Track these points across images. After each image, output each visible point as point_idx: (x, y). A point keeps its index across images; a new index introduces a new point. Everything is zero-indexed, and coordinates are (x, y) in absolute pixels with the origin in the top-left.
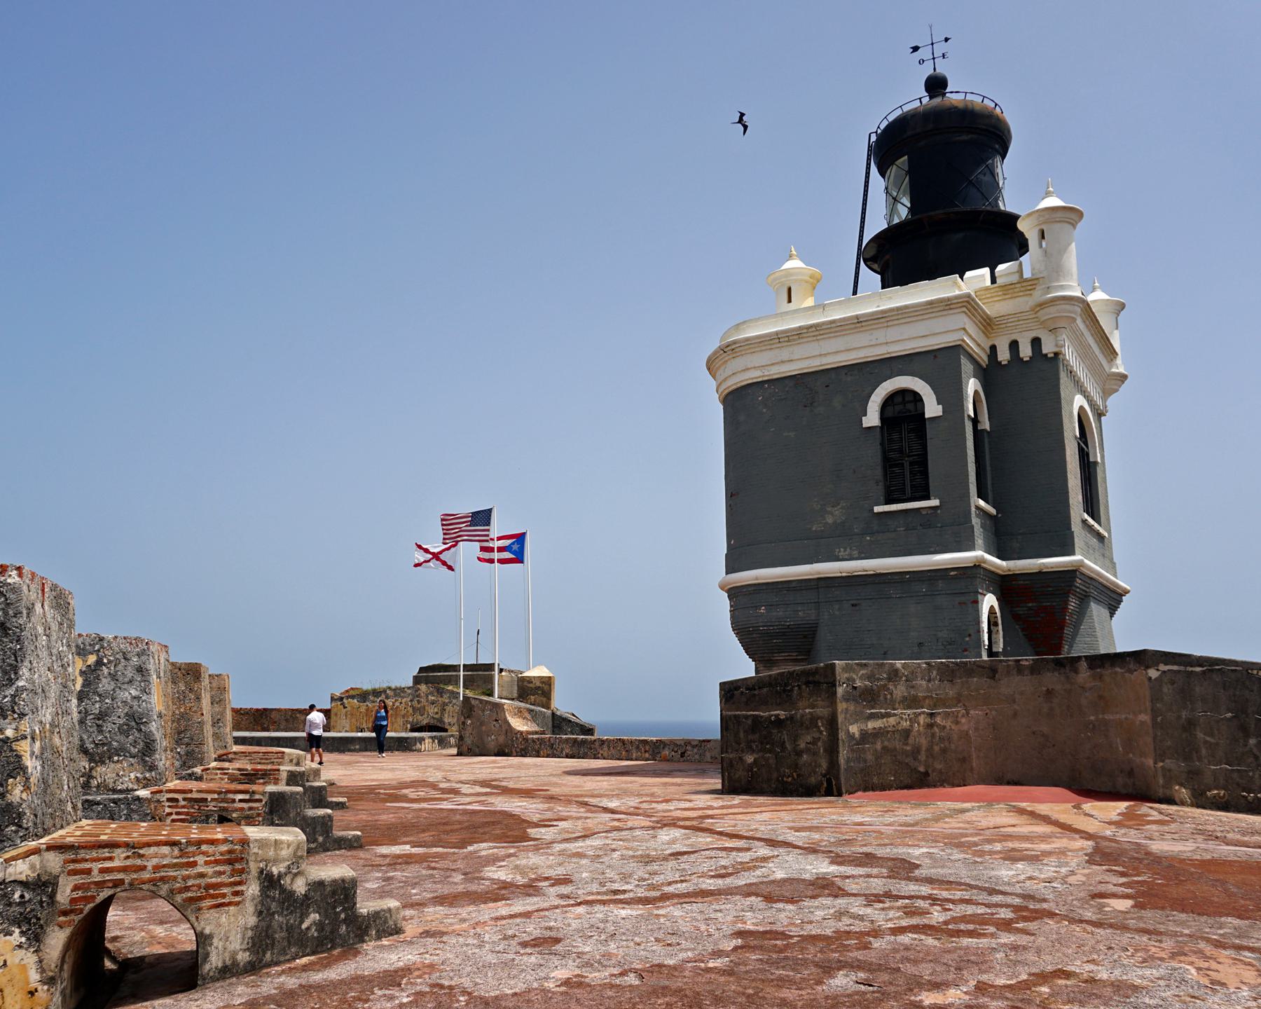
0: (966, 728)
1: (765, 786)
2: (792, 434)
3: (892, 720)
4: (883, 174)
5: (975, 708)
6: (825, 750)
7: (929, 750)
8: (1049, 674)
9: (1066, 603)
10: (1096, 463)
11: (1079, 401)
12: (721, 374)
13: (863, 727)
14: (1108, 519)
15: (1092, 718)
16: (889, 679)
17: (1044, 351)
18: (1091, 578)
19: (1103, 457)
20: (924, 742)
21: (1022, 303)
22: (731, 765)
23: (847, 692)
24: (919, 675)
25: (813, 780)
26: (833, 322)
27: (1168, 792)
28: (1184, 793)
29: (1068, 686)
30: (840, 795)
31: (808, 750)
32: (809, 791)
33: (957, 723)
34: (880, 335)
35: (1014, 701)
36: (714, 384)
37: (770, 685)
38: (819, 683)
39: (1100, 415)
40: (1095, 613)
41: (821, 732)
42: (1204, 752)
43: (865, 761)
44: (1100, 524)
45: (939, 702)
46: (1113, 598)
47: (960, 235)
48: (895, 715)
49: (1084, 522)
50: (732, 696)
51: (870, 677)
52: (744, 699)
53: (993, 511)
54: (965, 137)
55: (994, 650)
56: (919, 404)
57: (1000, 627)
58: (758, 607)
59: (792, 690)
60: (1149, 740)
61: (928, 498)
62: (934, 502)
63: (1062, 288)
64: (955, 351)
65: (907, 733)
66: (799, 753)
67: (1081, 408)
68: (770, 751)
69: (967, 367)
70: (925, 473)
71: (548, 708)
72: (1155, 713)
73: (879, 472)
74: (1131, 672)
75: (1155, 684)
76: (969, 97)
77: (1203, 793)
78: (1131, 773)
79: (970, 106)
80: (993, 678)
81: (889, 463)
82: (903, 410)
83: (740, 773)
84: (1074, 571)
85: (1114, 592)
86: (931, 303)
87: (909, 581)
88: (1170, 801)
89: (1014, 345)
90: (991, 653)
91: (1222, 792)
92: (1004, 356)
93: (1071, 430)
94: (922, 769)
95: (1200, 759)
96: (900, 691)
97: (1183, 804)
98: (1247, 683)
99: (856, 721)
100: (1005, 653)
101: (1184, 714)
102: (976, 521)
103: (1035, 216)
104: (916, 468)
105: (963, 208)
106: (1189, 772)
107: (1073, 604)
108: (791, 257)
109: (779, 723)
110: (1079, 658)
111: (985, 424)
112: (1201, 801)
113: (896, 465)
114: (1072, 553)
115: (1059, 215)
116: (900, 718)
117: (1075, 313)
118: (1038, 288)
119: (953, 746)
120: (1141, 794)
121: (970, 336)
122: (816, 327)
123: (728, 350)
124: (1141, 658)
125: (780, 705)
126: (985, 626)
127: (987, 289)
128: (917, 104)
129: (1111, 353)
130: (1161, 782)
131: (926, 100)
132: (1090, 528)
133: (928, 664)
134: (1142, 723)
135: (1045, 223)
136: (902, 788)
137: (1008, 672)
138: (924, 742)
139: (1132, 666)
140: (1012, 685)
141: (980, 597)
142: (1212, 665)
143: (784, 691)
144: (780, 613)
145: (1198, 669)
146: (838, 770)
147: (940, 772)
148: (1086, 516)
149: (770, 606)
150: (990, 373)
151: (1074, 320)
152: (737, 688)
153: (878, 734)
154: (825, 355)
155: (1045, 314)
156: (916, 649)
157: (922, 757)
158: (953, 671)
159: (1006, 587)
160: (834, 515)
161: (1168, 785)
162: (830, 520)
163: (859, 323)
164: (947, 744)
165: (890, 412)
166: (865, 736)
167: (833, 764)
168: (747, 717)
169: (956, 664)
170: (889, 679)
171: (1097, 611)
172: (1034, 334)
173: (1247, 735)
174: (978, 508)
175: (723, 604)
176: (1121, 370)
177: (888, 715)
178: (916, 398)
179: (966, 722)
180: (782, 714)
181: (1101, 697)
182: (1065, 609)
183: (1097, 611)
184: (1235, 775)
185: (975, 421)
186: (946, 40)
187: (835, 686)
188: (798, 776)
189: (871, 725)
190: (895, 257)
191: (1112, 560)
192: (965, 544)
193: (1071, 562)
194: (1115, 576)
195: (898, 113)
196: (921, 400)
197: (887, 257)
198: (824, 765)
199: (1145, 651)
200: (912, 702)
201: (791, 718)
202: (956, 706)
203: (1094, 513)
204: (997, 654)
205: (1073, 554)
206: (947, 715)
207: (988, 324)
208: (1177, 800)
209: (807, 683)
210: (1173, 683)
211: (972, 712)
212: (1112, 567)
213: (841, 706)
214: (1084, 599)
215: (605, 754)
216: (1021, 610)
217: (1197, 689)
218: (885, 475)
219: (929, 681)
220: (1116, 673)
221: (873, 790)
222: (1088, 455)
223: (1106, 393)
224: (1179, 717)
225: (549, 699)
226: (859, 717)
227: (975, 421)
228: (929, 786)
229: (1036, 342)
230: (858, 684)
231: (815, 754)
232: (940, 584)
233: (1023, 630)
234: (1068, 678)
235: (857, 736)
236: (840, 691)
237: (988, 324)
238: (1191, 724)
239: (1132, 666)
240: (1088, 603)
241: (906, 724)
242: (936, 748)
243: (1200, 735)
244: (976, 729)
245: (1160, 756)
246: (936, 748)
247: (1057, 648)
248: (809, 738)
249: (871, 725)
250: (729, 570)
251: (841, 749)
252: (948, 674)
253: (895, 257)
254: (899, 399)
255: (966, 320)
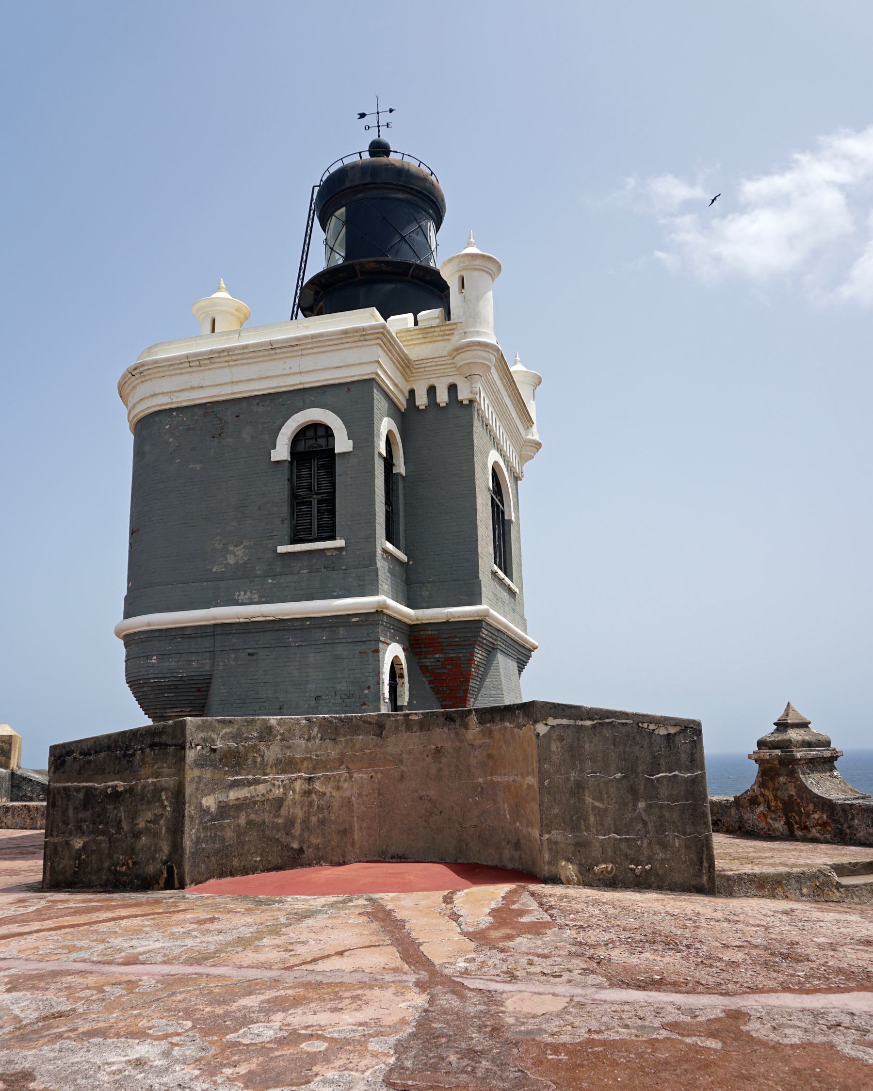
0: (348, 794)
1: (94, 878)
2: (198, 467)
3: (261, 788)
4: (324, 227)
5: (359, 770)
6: (167, 831)
7: (306, 821)
8: (438, 730)
9: (472, 654)
10: (510, 521)
11: (494, 456)
12: (132, 401)
13: (222, 797)
14: (521, 578)
15: (481, 780)
16: (261, 739)
17: (460, 398)
18: (499, 631)
19: (517, 517)
20: (299, 813)
21: (442, 348)
22: (55, 851)
23: (201, 756)
24: (297, 732)
25: (151, 869)
26: (246, 347)
27: (554, 869)
28: (569, 869)
29: (457, 744)
30: (182, 886)
31: (147, 830)
32: (146, 884)
33: (338, 788)
34: (293, 364)
35: (401, 761)
36: (125, 411)
37: (109, 748)
38: (166, 745)
39: (516, 479)
40: (502, 666)
41: (164, 807)
42: (592, 819)
43: (223, 840)
44: (512, 581)
45: (319, 765)
46: (523, 654)
47: (390, 286)
48: (265, 781)
49: (494, 573)
50: (63, 764)
51: (235, 737)
52: (76, 767)
53: (404, 558)
54: (400, 196)
55: (399, 704)
56: (330, 439)
57: (406, 679)
58: (149, 657)
59: (133, 755)
60: (536, 807)
61: (333, 538)
62: (339, 543)
63: (478, 333)
64: (369, 384)
65: (279, 802)
66: (137, 835)
67: (496, 463)
68: (102, 833)
69: (380, 404)
70: (332, 512)
71: (6, 766)
72: (542, 775)
73: (285, 510)
74: (520, 727)
75: (543, 742)
76: (406, 159)
77: (590, 869)
78: (517, 845)
79: (406, 166)
80: (380, 735)
81: (296, 501)
82: (313, 445)
83: (66, 863)
84: (481, 621)
85: (523, 646)
86: (345, 332)
87: (309, 628)
88: (555, 880)
89: (432, 391)
90: (395, 707)
91: (610, 866)
92: (421, 400)
93: (484, 484)
94: (295, 845)
95: (588, 829)
96: (273, 752)
97: (569, 882)
98: (638, 738)
99: (213, 791)
100: (410, 706)
101: (573, 775)
102: (382, 565)
103: (456, 261)
104: (324, 506)
105: (390, 258)
106: (577, 844)
107: (479, 656)
108: (219, 289)
109: (116, 796)
110: (470, 711)
111: (400, 468)
112: (589, 879)
113: (304, 503)
114: (479, 602)
115: (478, 262)
116: (272, 785)
117: (490, 360)
118: (456, 332)
119: (333, 817)
120: (524, 873)
121: (386, 372)
122: (228, 350)
123: (137, 373)
124: (530, 711)
125: (118, 774)
126: (386, 677)
127: (408, 330)
128: (356, 158)
129: (528, 421)
130: (547, 857)
131: (366, 156)
132: (501, 580)
133: (308, 720)
134: (530, 787)
135: (464, 269)
136: (270, 870)
137: (397, 728)
138: (299, 813)
139: (521, 720)
140: (403, 744)
141: (381, 645)
142: (603, 718)
143: (125, 755)
144: (172, 663)
145: (588, 723)
146: (182, 856)
147: (317, 847)
148: (496, 568)
149: (162, 656)
150: (407, 417)
151: (489, 368)
152: (69, 753)
153: (240, 806)
154: (237, 382)
155: (463, 359)
156: (313, 703)
157: (297, 831)
158: (336, 728)
159: (415, 638)
160: (236, 555)
161: (553, 862)
162: (231, 560)
163: (273, 349)
164: (326, 813)
165: (301, 447)
166: (224, 810)
167: (177, 847)
168: (78, 790)
169: (340, 719)
170: (261, 739)
171: (504, 664)
172: (450, 380)
173: (636, 800)
174: (385, 551)
175: (120, 651)
176: (536, 437)
177: (257, 782)
178: (328, 432)
179: (347, 788)
180: (120, 785)
181: (489, 756)
182: (471, 660)
183: (504, 664)
184: (623, 846)
185: (389, 462)
186: (391, 111)
187: (183, 748)
188: (134, 863)
189: (233, 795)
190: (321, 295)
191: (522, 617)
192: (368, 587)
193: (477, 612)
194: (526, 633)
195: (340, 165)
196: (333, 435)
197: (321, 304)
198: (166, 848)
199: (533, 701)
200: (287, 765)
201: (130, 790)
202: (338, 769)
203: (507, 571)
204: (402, 708)
205: (480, 603)
206: (328, 778)
207: (406, 366)
208: (563, 878)
209: (153, 745)
210: (561, 739)
211: (355, 775)
212: (523, 624)
213: (192, 774)
214: (491, 651)
215: (9, 823)
216: (428, 662)
217: (587, 746)
218: (292, 513)
219: (309, 740)
220: (505, 728)
221: (232, 875)
222: (503, 513)
223: (524, 459)
224: (568, 779)
225: (9, 758)
226: (213, 787)
227: (389, 462)
228: (302, 865)
229: (453, 389)
230: (219, 745)
231: (156, 835)
232: (342, 632)
233: (430, 682)
234: (457, 734)
235: (213, 809)
236: (191, 755)
237: (406, 366)
238: (579, 787)
239: (521, 720)
240: (495, 655)
241: (278, 792)
242: (314, 819)
243: (589, 800)
244: (360, 795)
245: (546, 828)
246: (314, 819)
247: (464, 701)
248: (149, 816)
249: (233, 795)
250: (127, 615)
251: (187, 828)
252: (331, 731)
253: (321, 295)
254: (310, 433)
255: (380, 352)
